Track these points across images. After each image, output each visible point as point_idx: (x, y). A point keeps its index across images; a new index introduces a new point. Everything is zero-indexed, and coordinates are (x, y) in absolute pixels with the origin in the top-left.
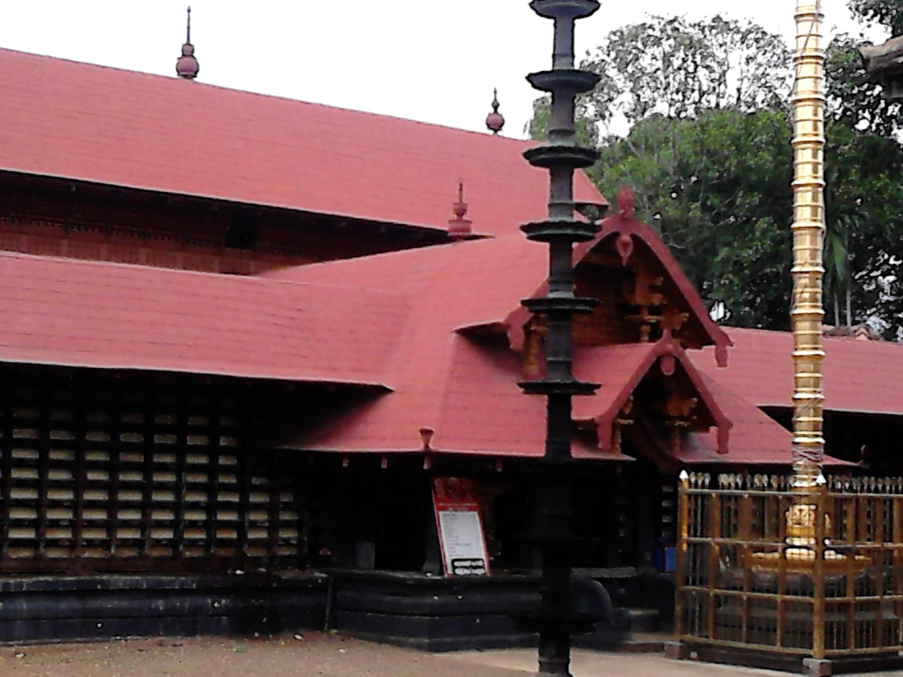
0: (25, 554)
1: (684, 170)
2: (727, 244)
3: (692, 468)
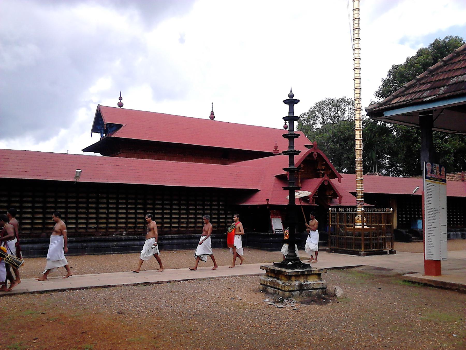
0: (176, 230)
1: (335, 136)
2: (346, 154)
3: (331, 207)
